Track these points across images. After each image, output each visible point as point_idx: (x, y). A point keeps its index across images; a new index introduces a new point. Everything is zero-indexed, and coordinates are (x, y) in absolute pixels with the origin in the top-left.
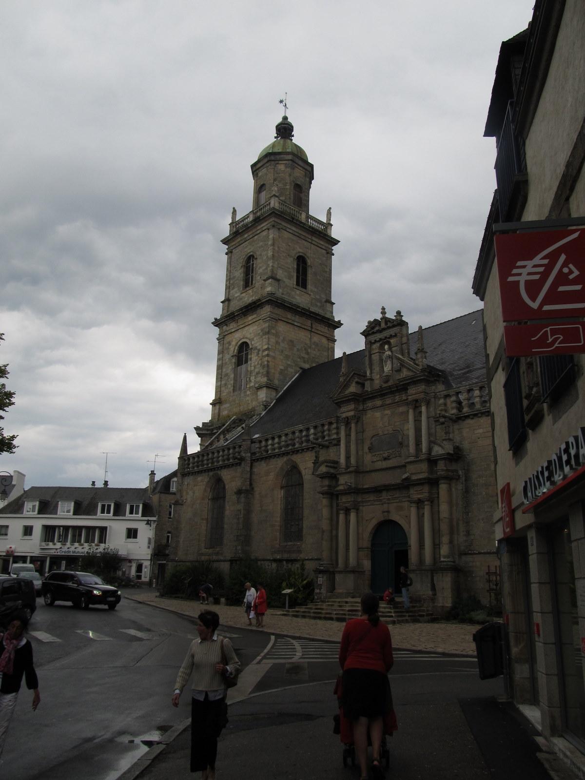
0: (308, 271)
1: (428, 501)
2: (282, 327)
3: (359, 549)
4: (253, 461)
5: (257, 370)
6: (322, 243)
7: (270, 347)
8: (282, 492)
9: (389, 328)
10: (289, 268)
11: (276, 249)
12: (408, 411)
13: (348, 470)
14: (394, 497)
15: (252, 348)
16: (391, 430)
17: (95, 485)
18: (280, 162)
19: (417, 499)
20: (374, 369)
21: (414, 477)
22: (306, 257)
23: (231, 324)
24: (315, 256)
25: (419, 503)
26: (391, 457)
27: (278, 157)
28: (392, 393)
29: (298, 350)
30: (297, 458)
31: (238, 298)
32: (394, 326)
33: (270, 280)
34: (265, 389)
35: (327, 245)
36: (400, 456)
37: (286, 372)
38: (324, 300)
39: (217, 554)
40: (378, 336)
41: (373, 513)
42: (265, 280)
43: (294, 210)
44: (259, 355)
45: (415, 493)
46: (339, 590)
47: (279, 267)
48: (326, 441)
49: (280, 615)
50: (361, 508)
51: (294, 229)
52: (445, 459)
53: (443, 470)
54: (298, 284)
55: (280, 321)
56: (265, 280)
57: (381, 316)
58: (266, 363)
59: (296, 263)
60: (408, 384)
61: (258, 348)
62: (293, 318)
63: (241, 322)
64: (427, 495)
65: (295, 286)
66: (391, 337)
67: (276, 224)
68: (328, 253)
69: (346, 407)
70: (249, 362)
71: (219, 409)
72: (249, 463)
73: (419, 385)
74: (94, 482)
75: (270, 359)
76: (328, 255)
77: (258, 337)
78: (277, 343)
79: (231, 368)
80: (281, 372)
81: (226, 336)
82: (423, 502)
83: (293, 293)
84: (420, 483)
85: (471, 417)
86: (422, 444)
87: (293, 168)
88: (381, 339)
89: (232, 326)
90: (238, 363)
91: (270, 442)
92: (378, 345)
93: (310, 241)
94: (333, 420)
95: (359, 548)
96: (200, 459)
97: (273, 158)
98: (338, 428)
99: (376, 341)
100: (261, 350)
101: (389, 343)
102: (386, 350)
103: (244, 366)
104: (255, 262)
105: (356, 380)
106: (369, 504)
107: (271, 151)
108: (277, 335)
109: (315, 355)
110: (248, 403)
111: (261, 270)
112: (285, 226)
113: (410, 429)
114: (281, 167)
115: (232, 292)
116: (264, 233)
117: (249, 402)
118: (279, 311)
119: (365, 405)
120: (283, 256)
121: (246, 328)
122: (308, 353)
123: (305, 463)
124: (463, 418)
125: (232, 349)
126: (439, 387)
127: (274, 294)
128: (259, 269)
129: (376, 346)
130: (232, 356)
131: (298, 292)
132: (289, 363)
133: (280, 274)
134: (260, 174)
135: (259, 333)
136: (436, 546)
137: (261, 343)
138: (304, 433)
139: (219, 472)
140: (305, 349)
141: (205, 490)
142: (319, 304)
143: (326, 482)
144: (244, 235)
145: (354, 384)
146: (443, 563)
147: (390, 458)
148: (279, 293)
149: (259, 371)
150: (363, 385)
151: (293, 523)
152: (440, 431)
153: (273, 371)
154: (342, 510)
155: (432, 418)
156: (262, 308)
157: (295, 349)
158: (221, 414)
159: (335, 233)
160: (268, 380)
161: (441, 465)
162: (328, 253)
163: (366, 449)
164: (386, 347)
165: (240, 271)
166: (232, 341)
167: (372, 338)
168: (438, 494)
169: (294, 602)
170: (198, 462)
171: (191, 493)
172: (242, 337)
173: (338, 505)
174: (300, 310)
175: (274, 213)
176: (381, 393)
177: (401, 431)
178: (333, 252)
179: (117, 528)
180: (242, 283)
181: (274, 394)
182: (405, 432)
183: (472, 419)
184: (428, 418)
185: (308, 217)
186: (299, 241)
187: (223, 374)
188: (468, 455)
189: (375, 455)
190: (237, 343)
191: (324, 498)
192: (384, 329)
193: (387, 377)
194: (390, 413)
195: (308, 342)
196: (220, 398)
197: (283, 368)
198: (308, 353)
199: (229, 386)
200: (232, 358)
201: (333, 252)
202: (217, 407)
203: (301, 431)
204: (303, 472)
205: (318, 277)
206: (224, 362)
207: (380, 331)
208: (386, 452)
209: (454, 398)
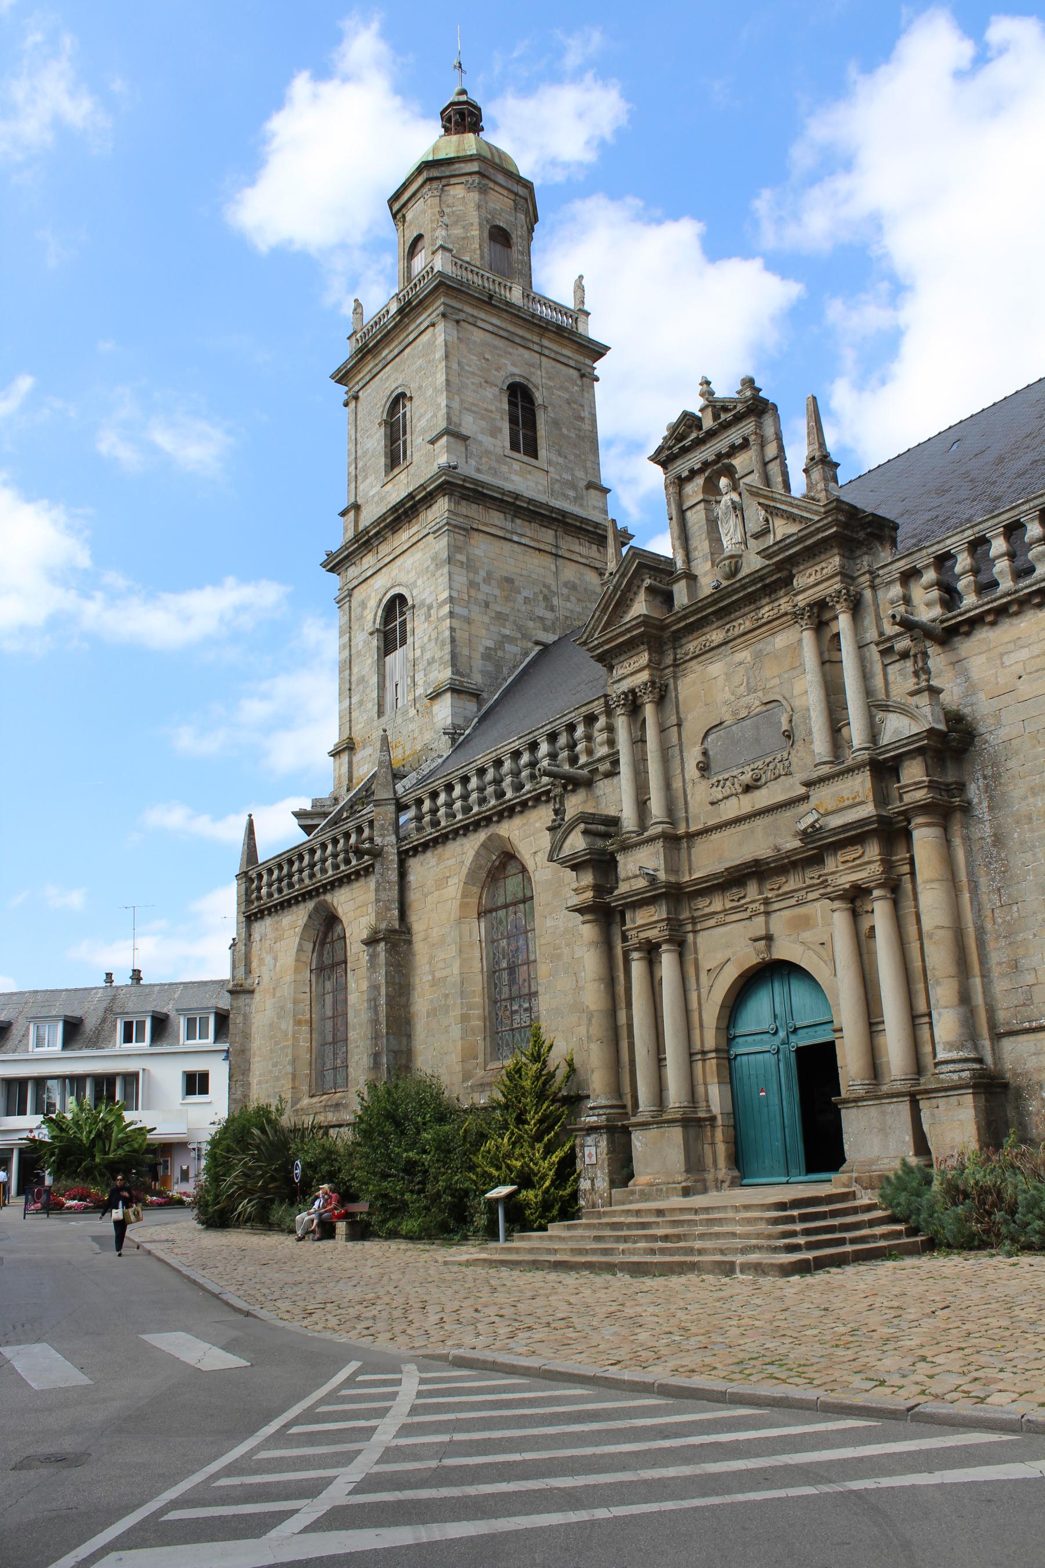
0: (537, 417)
1: (880, 886)
2: (481, 548)
3: (692, 1056)
4: (403, 857)
5: (428, 655)
6: (565, 352)
7: (455, 594)
8: (482, 925)
9: (725, 426)
10: (491, 412)
11: (455, 366)
12: (800, 640)
13: (646, 834)
14: (781, 891)
15: (413, 607)
16: (757, 703)
17: (112, 982)
18: (453, 181)
19: (847, 886)
20: (696, 549)
21: (836, 821)
22: (530, 386)
23: (365, 560)
24: (552, 384)
25: (855, 898)
26: (763, 780)
27: (446, 171)
28: (751, 599)
29: (527, 601)
30: (511, 830)
31: (376, 499)
32: (738, 418)
33: (445, 438)
34: (448, 695)
35: (581, 358)
36: (788, 774)
37: (500, 653)
38: (582, 484)
39: (337, 1106)
40: (695, 459)
41: (725, 947)
42: (432, 442)
43: (488, 278)
44: (432, 619)
45: (843, 871)
46: (642, 1179)
47: (466, 409)
48: (581, 767)
49: (468, 1263)
50: (690, 937)
51: (495, 321)
52: (920, 751)
53: (917, 786)
54: (514, 446)
55: (475, 534)
56: (432, 442)
57: (701, 402)
58: (447, 633)
59: (505, 400)
60: (792, 561)
61: (428, 602)
62: (509, 525)
63: (384, 549)
64: (876, 868)
65: (508, 452)
66: (734, 450)
67: (450, 310)
68: (583, 376)
69: (626, 664)
70: (409, 640)
71: (350, 763)
72: (392, 860)
73: (823, 557)
74: (109, 975)
75: (456, 624)
76: (585, 379)
77: (425, 578)
78: (472, 584)
79: (369, 661)
80: (488, 655)
81: (356, 591)
82: (868, 891)
83: (504, 468)
84: (853, 837)
85: (989, 618)
86: (849, 724)
87: (483, 190)
88: (706, 465)
89: (369, 561)
90: (386, 646)
91: (442, 798)
92: (700, 481)
93: (536, 348)
94: (598, 707)
95: (691, 1055)
96: (285, 871)
97: (435, 173)
98: (610, 729)
99: (693, 473)
100: (435, 604)
101: (729, 471)
102: (724, 491)
103: (399, 653)
104: (408, 409)
105: (648, 582)
106: (712, 922)
107: (431, 159)
108: (469, 566)
109: (572, 611)
110: (414, 739)
111: (423, 423)
112: (473, 316)
113: (808, 693)
114: (457, 192)
115: (361, 488)
116: (425, 337)
117: (416, 733)
118: (473, 511)
119: (678, 651)
120: (473, 383)
121: (398, 562)
122: (552, 609)
123: (529, 835)
124: (964, 629)
125: (370, 617)
126: (883, 554)
127: (455, 468)
128: (419, 420)
129: (694, 490)
130: (371, 634)
131: (516, 466)
132: (508, 632)
133: (468, 425)
134: (409, 216)
135: (428, 567)
136: (917, 1020)
137: (432, 588)
138: (525, 758)
139: (328, 897)
140: (546, 598)
141: (300, 949)
142: (571, 493)
143: (588, 878)
144: (380, 352)
145: (642, 596)
146: (944, 1068)
147: (759, 783)
148: (468, 469)
149: (433, 658)
150: (668, 598)
151: (515, 1008)
152: (901, 680)
153: (465, 651)
154: (636, 949)
155: (873, 647)
156: (430, 506)
157: (520, 599)
158: (355, 775)
159: (595, 330)
160: (453, 673)
161: (913, 772)
162: (583, 376)
163: (692, 771)
164: (724, 482)
165: (379, 434)
166: (369, 598)
167: (683, 466)
168: (912, 862)
169: (518, 1218)
170: (280, 880)
171: (268, 959)
172: (389, 585)
173: (625, 939)
174: (525, 505)
175: (444, 286)
176: (722, 607)
177: (784, 702)
178: (596, 372)
179: (165, 1076)
180: (382, 461)
181: (471, 706)
182: (797, 703)
183: (993, 624)
184: (861, 647)
185: (528, 293)
186: (511, 350)
187: (354, 678)
188: (991, 732)
189: (719, 781)
190: (381, 600)
191: (584, 923)
192: (712, 434)
193: (733, 561)
194: (749, 659)
195: (550, 581)
196: (350, 739)
197: (493, 646)
198: (552, 609)
199: (369, 705)
200: (370, 637)
201: (596, 372)
202: (345, 757)
203: (516, 755)
204: (530, 865)
205: (565, 431)
206: (353, 651)
207: (699, 442)
208: (747, 769)
209: (930, 575)
